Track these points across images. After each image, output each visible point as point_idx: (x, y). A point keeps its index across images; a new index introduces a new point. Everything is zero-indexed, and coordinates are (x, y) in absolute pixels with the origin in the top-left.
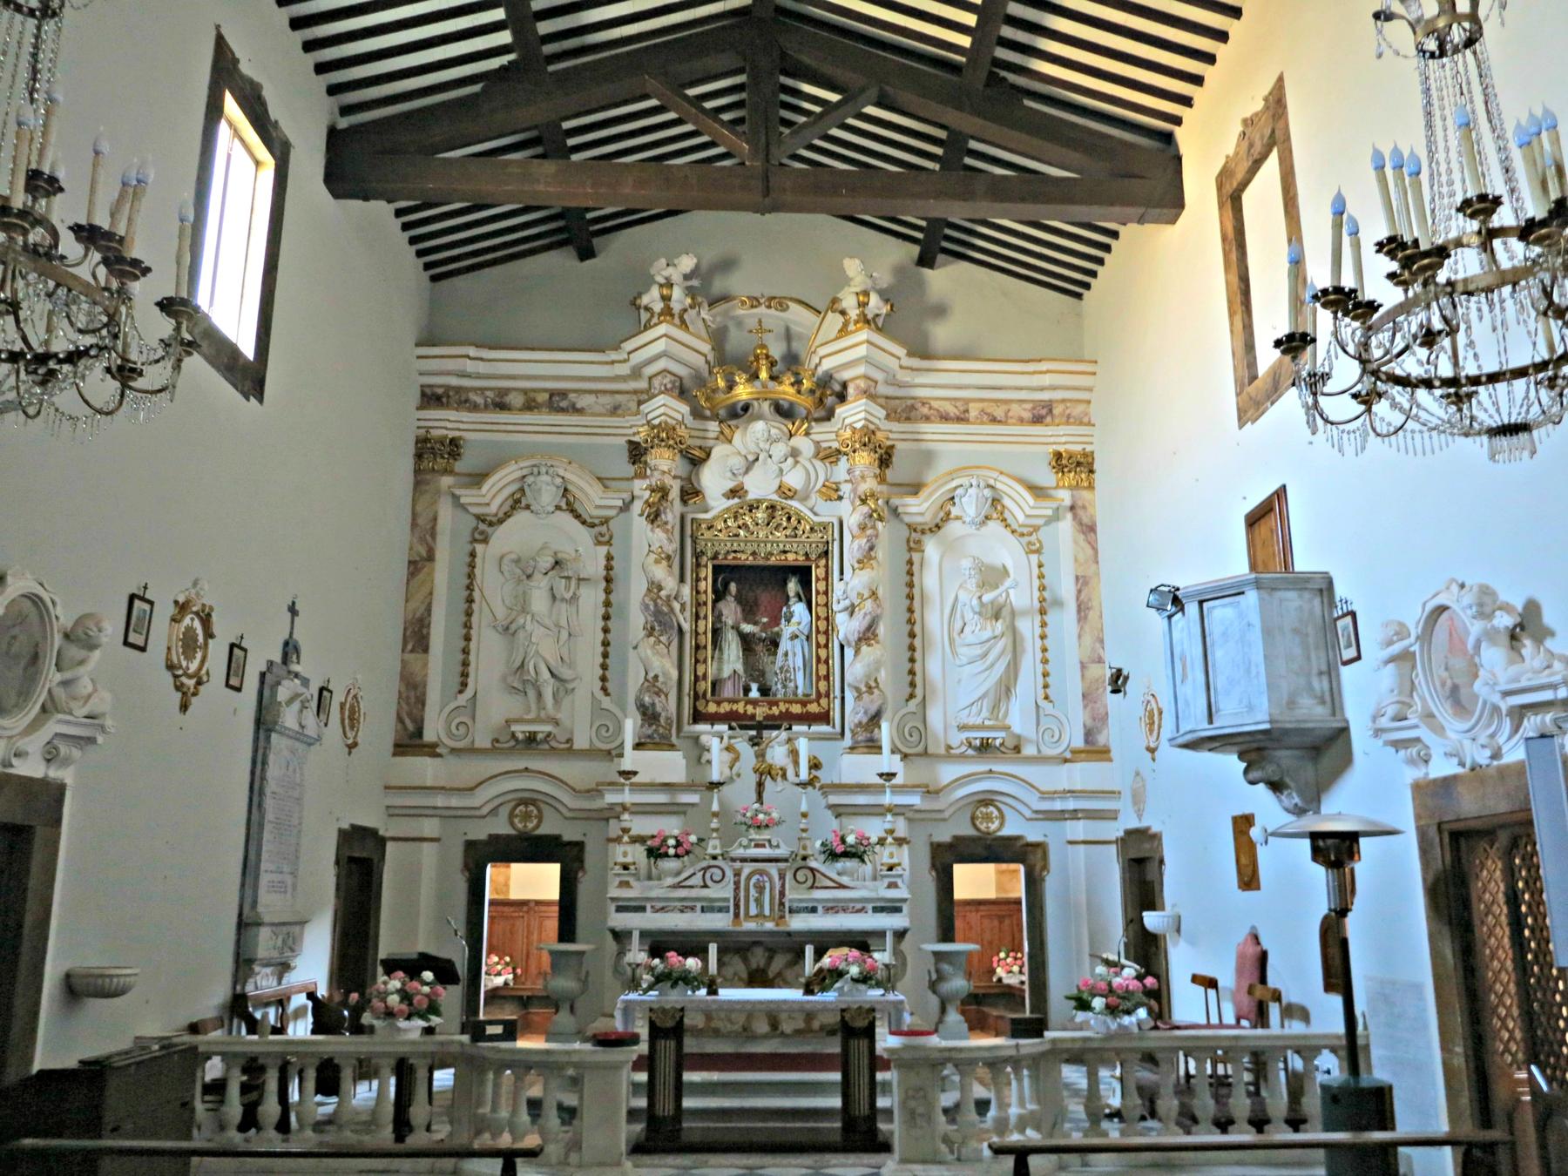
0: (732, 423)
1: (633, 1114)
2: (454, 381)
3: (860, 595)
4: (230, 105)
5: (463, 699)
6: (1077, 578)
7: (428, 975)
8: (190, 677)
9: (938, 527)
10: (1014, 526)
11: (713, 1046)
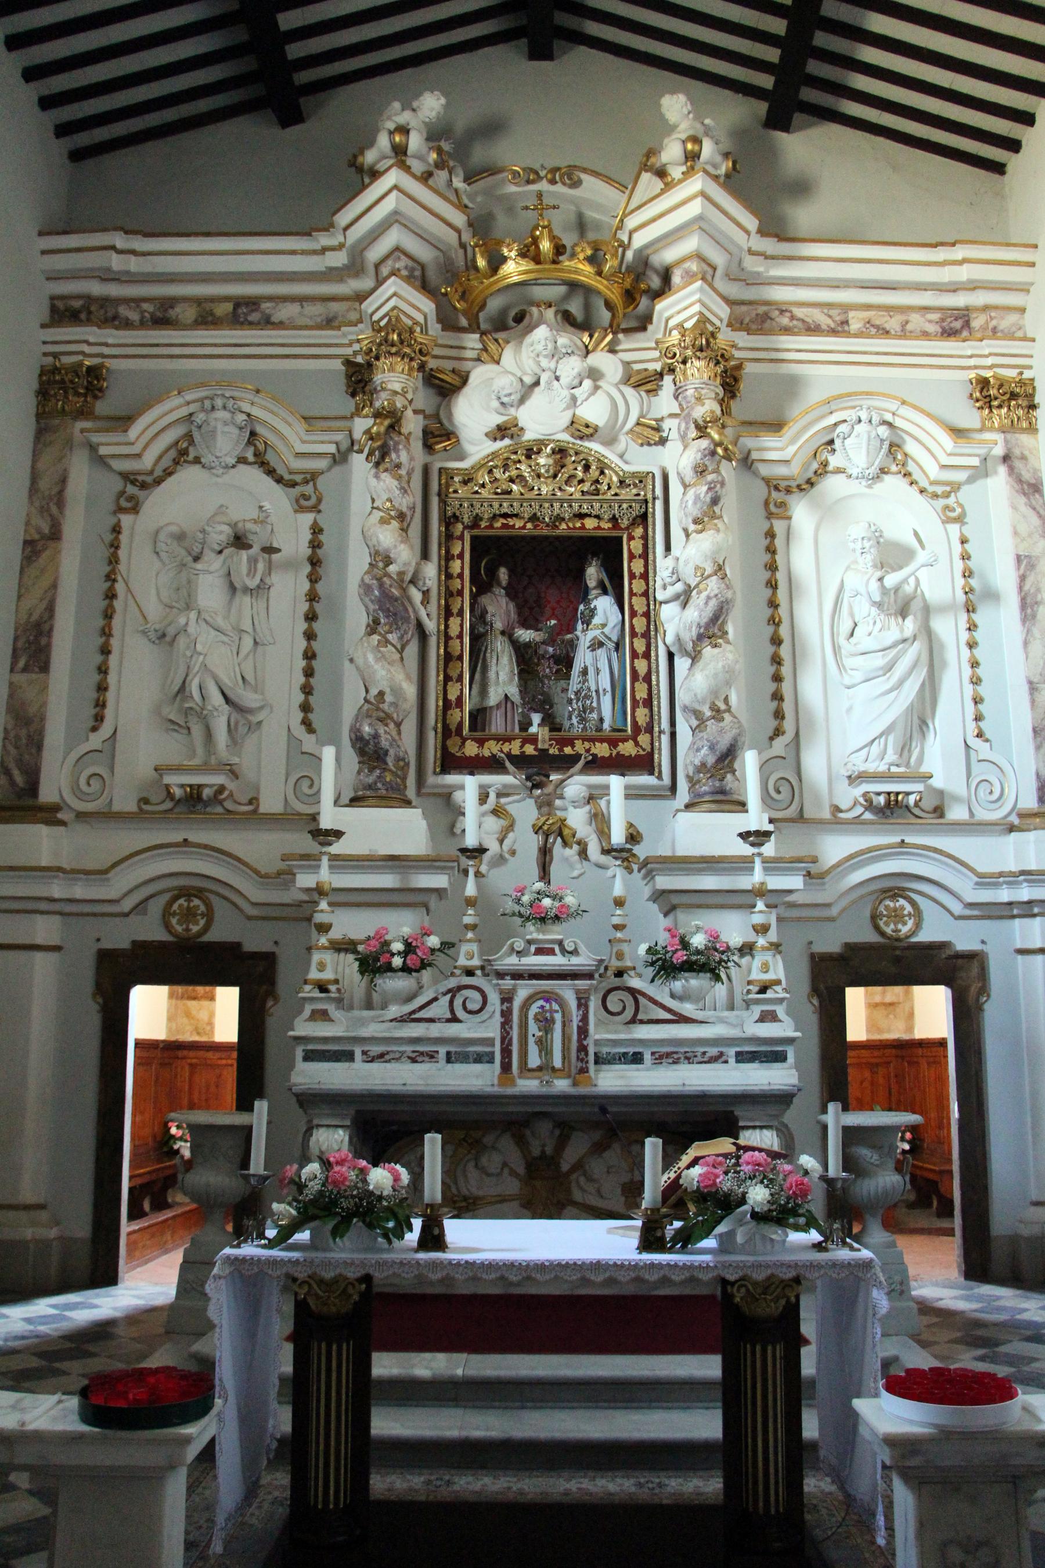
0: (501, 336)
2: (96, 289)
5: (96, 740)
6: (1019, 559)
9: (811, 483)
10: (924, 483)
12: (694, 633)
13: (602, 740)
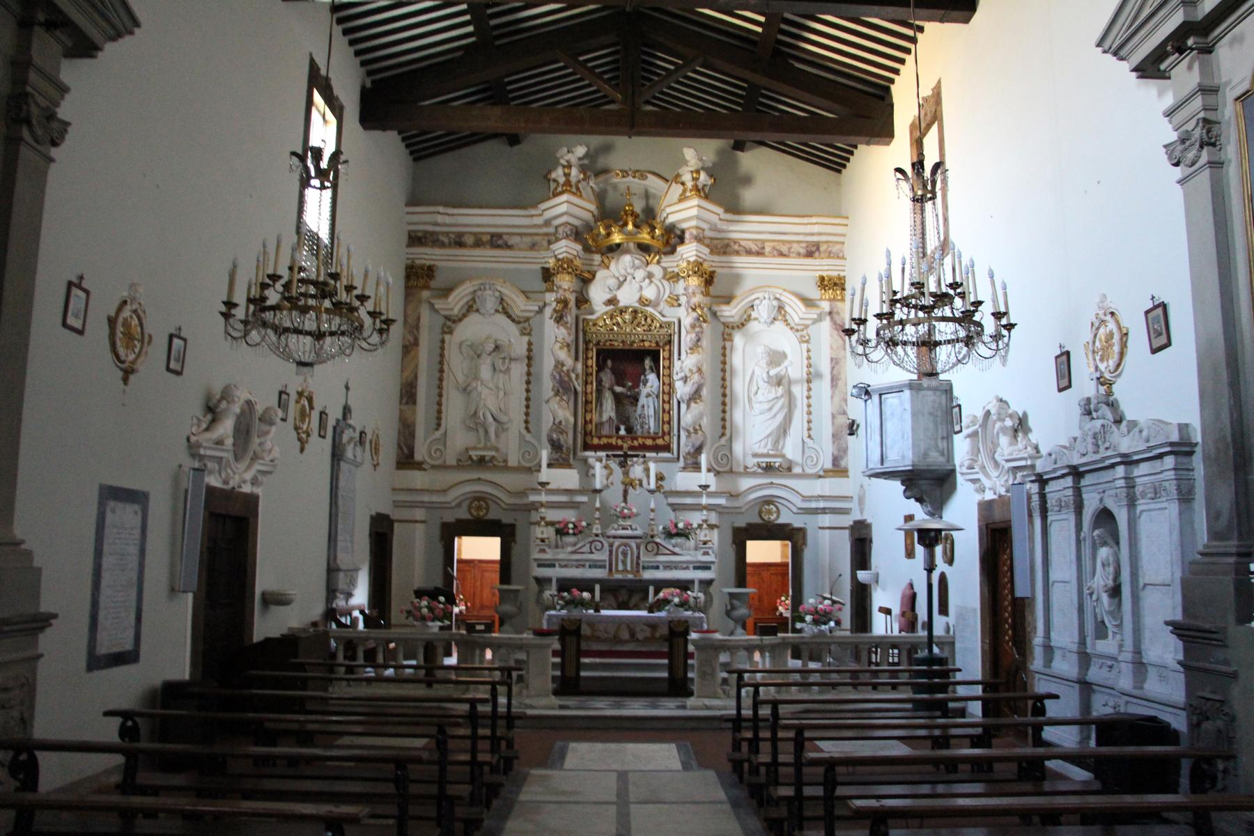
2: (430, 228)
3: (691, 370)
4: (317, 97)
5: (438, 434)
7: (442, 599)
9: (743, 325)
10: (792, 325)
11: (596, 647)
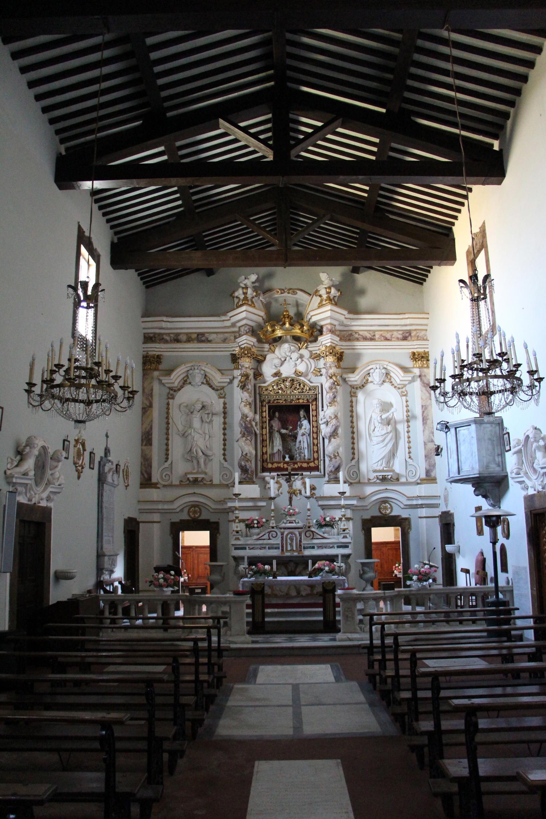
1: (248, 623)
2: (158, 331)
5: (167, 465)
6: (422, 406)
7: (172, 572)
8: (79, 466)
9: (363, 386)
10: (396, 385)
11: (274, 601)
12: (329, 434)
13: (305, 462)
